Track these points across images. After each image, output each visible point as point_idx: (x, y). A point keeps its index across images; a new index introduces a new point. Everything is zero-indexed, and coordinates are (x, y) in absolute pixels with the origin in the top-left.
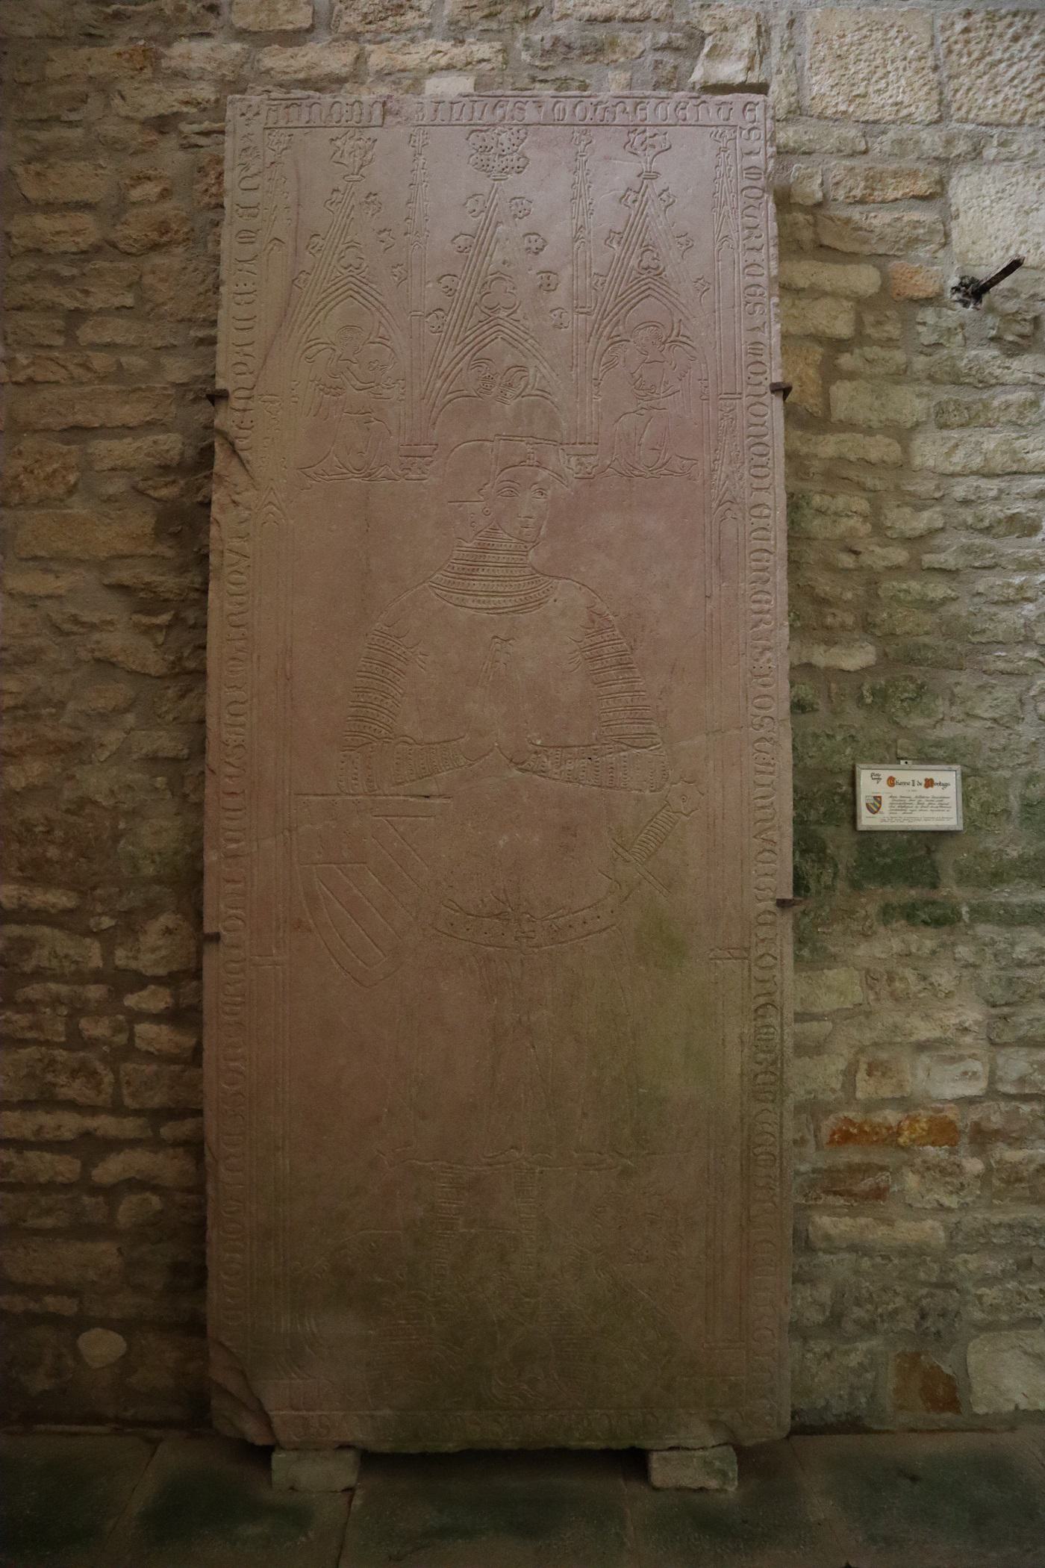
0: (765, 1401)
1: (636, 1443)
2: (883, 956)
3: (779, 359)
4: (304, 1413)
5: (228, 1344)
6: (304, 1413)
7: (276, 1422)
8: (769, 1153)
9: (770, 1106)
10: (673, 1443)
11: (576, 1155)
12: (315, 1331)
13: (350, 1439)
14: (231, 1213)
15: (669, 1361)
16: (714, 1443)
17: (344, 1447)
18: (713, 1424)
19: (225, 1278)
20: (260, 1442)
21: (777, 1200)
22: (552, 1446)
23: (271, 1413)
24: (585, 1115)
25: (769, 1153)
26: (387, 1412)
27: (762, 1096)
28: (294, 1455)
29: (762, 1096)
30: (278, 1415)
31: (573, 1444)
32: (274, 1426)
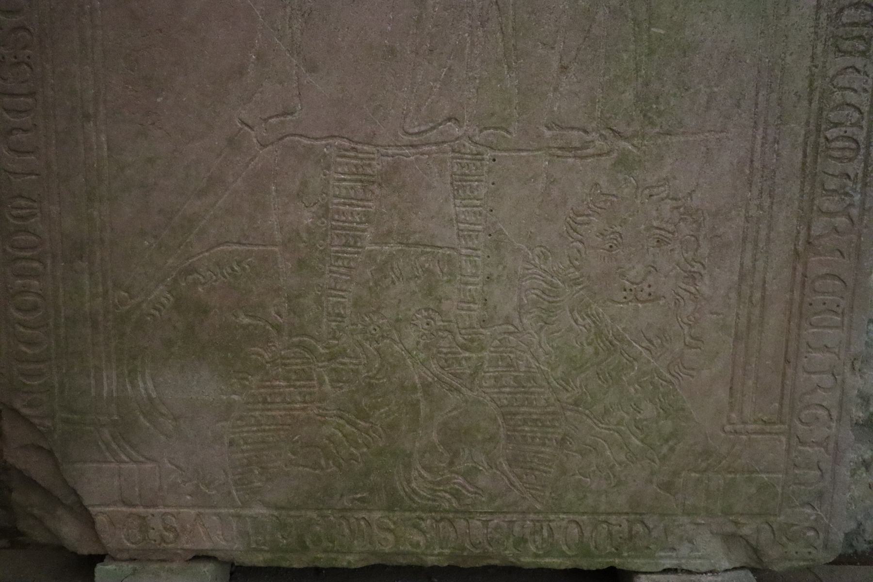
0: (808, 510)
1: (617, 562)
2: (352, 461)
3: (303, 512)
4: (141, 510)
5: (25, 411)
6: (141, 510)
7: (101, 520)
8: (850, 138)
9: (859, 62)
10: (668, 564)
11: (548, 134)
12: (154, 395)
13: (206, 545)
14: (21, 218)
15: (672, 449)
16: (726, 565)
17: (200, 557)
18: (730, 539)
19: (19, 315)
20: (85, 549)
21: (854, 212)
22: (497, 562)
23: (93, 510)
24: (564, 68)
25: (850, 138)
26: (258, 510)
27: (846, 45)
28: (127, 567)
29: (846, 45)
30: (102, 514)
31: (527, 561)
32: (98, 526)
